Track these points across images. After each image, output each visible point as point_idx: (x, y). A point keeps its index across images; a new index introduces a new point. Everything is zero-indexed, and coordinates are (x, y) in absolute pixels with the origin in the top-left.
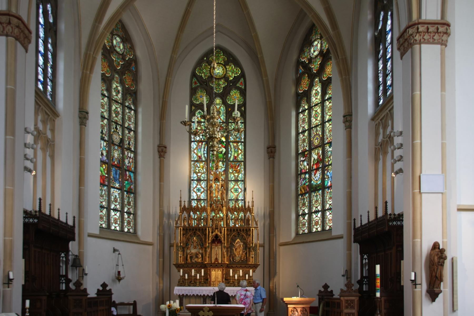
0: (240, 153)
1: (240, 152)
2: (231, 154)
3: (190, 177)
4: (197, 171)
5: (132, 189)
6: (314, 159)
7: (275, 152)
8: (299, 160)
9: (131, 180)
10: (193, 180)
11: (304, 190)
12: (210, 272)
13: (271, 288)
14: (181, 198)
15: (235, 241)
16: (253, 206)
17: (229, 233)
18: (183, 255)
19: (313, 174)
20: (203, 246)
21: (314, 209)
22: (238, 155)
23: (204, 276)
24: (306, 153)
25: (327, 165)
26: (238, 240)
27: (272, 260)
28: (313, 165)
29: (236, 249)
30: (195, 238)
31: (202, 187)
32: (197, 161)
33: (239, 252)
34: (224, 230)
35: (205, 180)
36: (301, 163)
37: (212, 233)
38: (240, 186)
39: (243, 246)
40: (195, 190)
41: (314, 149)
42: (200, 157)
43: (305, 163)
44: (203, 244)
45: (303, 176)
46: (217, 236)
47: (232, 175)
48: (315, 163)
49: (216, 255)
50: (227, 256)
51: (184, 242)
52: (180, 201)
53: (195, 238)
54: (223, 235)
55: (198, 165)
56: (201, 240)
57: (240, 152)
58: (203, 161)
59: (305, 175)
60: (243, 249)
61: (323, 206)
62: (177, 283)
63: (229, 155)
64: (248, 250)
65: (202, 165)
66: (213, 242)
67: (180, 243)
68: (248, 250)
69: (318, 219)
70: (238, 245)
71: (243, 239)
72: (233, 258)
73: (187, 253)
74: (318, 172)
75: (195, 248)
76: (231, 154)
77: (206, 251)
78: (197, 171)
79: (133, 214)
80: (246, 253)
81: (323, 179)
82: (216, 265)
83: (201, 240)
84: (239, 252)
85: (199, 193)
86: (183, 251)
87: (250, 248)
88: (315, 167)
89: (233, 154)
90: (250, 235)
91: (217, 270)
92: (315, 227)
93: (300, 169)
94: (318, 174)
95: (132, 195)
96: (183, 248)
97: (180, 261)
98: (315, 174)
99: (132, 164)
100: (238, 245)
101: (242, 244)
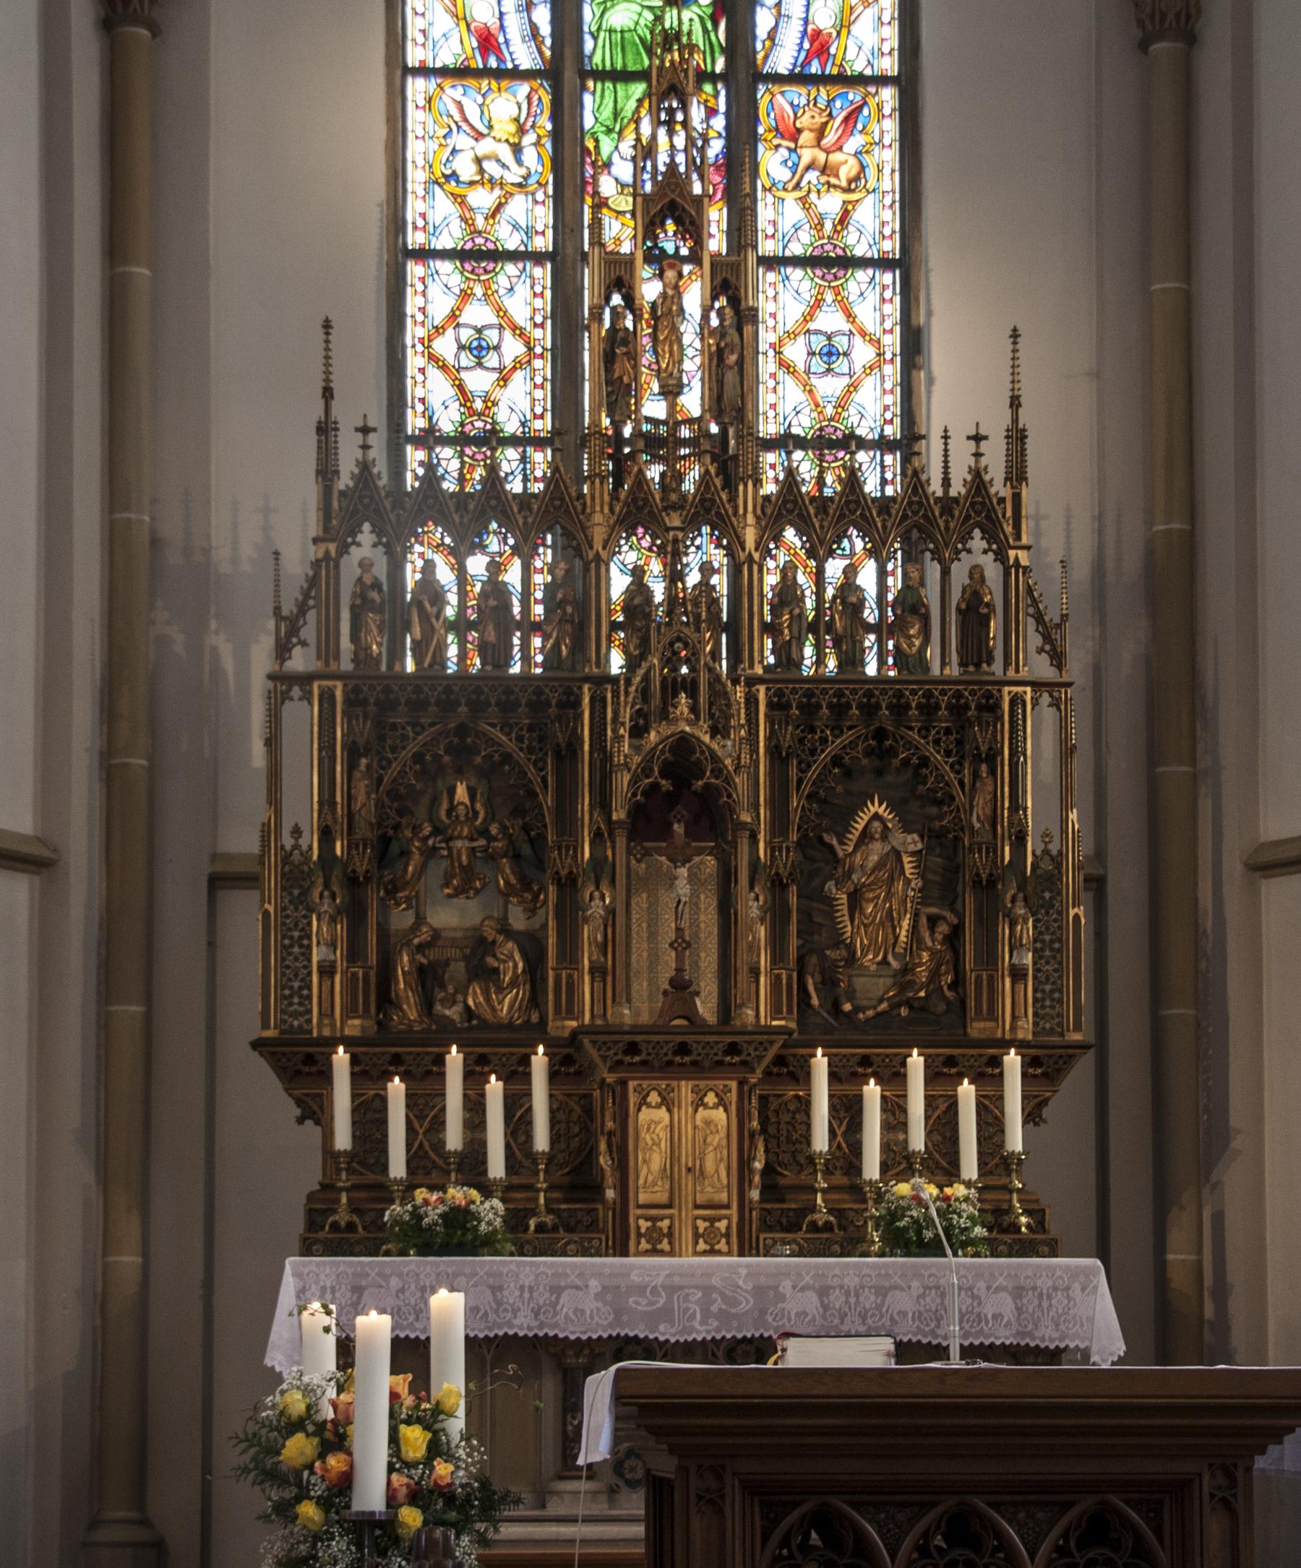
3: (396, 223)
4: (466, 170)
10: (424, 254)
12: (623, 1117)
13: (1179, 1279)
14: (328, 393)
15: (842, 824)
16: (1016, 473)
17: (788, 735)
18: (354, 954)
20: (540, 865)
23: (550, 1158)
26: (877, 808)
27: (1179, 1012)
29: (855, 901)
30: (461, 792)
31: (506, 322)
32: (460, 73)
33: (884, 932)
34: (751, 701)
35: (537, 258)
37: (638, 732)
38: (866, 313)
39: (922, 871)
40: (445, 346)
42: (487, 42)
44: (537, 842)
46: (682, 760)
47: (792, 212)
49: (682, 944)
50: (778, 956)
51: (363, 831)
52: (326, 429)
53: (461, 792)
54: (743, 757)
56: (522, 805)
58: (517, 74)
59: (913, 636)
60: (925, 896)
62: (299, 1225)
64: (969, 903)
66: (648, 822)
67: (326, 835)
68: (969, 903)
70: (876, 851)
71: (926, 806)
72: (828, 982)
73: (383, 932)
77: (569, 915)
78: (466, 170)
80: (957, 931)
82: (679, 1051)
83: (522, 805)
84: (884, 932)
86: (355, 914)
87: (987, 887)
90: (992, 757)
91: (685, 1090)
96: (353, 883)
97: (326, 1013)
100: (876, 851)
101: (913, 842)
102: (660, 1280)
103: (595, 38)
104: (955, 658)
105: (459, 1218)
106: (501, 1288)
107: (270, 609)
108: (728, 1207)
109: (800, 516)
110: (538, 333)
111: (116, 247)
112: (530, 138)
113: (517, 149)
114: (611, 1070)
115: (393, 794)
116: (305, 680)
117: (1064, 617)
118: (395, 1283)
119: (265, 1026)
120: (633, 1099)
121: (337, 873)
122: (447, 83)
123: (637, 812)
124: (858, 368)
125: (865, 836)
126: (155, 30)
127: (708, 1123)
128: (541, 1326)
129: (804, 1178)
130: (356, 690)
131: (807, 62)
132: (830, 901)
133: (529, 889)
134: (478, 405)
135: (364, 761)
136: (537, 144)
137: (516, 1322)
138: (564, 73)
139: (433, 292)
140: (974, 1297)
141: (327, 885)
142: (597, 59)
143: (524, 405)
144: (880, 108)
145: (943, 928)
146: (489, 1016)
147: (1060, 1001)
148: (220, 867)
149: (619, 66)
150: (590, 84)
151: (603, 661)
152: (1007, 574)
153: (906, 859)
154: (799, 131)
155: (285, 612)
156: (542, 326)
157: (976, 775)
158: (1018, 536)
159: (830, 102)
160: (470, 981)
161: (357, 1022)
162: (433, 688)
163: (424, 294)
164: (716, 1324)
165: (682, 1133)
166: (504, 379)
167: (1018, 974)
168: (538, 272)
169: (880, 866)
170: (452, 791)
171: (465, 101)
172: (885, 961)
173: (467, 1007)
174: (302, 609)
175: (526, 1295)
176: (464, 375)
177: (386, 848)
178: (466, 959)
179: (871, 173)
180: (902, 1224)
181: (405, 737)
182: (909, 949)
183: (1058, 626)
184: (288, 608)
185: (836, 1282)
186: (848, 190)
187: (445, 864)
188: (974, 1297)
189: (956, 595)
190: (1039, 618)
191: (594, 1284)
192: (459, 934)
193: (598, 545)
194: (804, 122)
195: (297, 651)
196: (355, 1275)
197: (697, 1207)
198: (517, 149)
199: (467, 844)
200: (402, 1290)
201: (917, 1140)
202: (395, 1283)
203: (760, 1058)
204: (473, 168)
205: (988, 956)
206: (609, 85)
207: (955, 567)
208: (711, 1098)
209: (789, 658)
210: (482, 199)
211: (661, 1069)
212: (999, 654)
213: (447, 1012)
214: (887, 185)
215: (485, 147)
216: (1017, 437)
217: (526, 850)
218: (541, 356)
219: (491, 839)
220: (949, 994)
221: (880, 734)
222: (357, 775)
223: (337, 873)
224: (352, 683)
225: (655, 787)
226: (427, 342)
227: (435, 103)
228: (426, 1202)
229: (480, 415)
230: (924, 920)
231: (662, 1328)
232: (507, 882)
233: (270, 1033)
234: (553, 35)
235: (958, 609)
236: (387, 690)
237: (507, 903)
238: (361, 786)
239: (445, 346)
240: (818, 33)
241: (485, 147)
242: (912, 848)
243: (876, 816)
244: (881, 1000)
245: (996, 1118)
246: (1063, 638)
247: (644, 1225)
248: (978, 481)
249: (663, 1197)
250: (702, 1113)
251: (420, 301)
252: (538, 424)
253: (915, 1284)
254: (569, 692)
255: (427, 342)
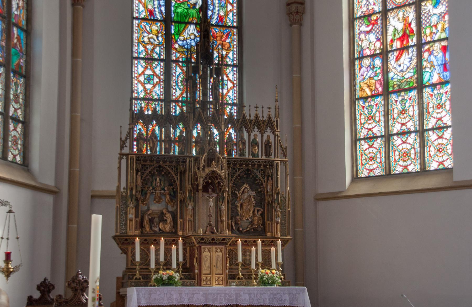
0: (231, 11)
1: (230, 7)
2: (213, 11)
4: (146, 40)
5: (21, 67)
6: (395, 29)
7: (303, 12)
8: (357, 31)
9: (21, 47)
10: (137, 58)
11: (371, 90)
12: (200, 254)
18: (137, 216)
19: (392, 57)
21: (396, 128)
22: (227, 14)
24: (374, 18)
25: (429, 43)
28: (392, 41)
35: (162, 60)
36: (362, 36)
41: (393, 9)
42: (151, 13)
43: (372, 37)
45: (367, 62)
48: (397, 36)
55: (148, 29)
57: (230, 7)
58: (158, 21)
60: (256, 205)
61: (422, 123)
63: (210, 13)
65: (155, 28)
69: (409, 146)
70: (246, 195)
71: (257, 186)
72: (236, 224)
74: (405, 54)
75: (158, 200)
76: (213, 11)
78: (146, 40)
79: (23, 123)
81: (420, 69)
84: (248, 215)
85: (149, 86)
87: (270, 204)
88: (397, 44)
89: (217, 12)
91: (214, 248)
92: (401, 163)
93: (357, 49)
94: (409, 59)
95: (22, 80)
98: (398, 59)
99: (22, 11)
101: (253, 193)
102: (215, 292)
103: (174, 14)
104: (264, 154)
105: (170, 278)
106: (181, 294)
107: (119, 138)
108: (222, 274)
109: (233, 123)
110: (162, 77)
111: (74, 54)
112: (160, 35)
113: (157, 37)
114: (197, 244)
115: (144, 180)
116: (127, 155)
117: (286, 147)
118: (158, 293)
119: (117, 232)
120: (202, 250)
121: (134, 198)
122: (142, 21)
123: (204, 187)
124: (229, 88)
125: (243, 192)
126: (83, 6)
127: (218, 256)
128: (190, 302)
129: (134, 267)
130: (138, 157)
131: (219, 22)
132: (236, 206)
133: (172, 202)
134: (149, 92)
135: (139, 173)
136: (162, 36)
137: (163, 302)
138: (167, 21)
139: (139, 67)
140: (281, 295)
141: (132, 201)
142: (175, 18)
143: (158, 92)
144: (234, 33)
145: (260, 212)
146: (164, 230)
147: (286, 229)
148: (93, 194)
149: (179, 20)
150: (173, 24)
151: (191, 152)
152: (275, 137)
153: (252, 197)
154: (217, 37)
155: (123, 139)
156: (162, 75)
157: (268, 180)
158: (278, 129)
159: (223, 31)
160: (159, 222)
161: (137, 231)
162: (155, 157)
163: (137, 67)
164: (227, 301)
165: (212, 257)
166: (154, 86)
167: (277, 223)
168: (162, 64)
169: (247, 198)
170: (156, 180)
171: (146, 26)
172: (248, 219)
173: (159, 228)
174: (126, 139)
175: (165, 296)
176: (145, 85)
177: (143, 192)
178: (159, 217)
179: (232, 47)
180: (264, 279)
181: (147, 168)
182: (253, 216)
183: (285, 148)
184: (123, 139)
185: (252, 292)
186: (227, 50)
187: (154, 196)
188: (281, 295)
189: (264, 141)
190: (281, 146)
191: (201, 293)
192: (157, 212)
193: (191, 128)
194: (218, 35)
195: (125, 148)
196: (150, 291)
197: (216, 274)
198: (157, 37)
199: (159, 192)
200: (160, 294)
201: (162, 259)
202: (158, 293)
203: (229, 242)
204: (148, 40)
205: (270, 218)
206: (177, 24)
207: (264, 135)
208: (219, 250)
209: (230, 153)
210: (149, 47)
211: (208, 244)
212: (273, 154)
213: (156, 229)
214: (235, 50)
215: (151, 36)
216: (276, 108)
217: (172, 193)
218: (162, 82)
219: (165, 190)
220: (261, 227)
221: (248, 170)
222: (138, 176)
223: (134, 198)
224: (137, 156)
225: (208, 181)
226: (138, 77)
227: (140, 26)
228: (163, 274)
229: (149, 94)
230: (256, 211)
231: (216, 302)
232: (168, 201)
233: (118, 234)
234: (165, 13)
235: (265, 144)
236: (145, 157)
237: (168, 204)
238: (139, 178)
239: (142, 79)
240: (221, 16)
241: (151, 36)
242: (253, 195)
243: (246, 188)
244: (247, 228)
245: (235, 253)
246: (286, 151)
247: (204, 278)
248: (269, 118)
249: (208, 272)
250: (217, 253)
251: (136, 69)
252: (162, 97)
253: (268, 292)
254: (184, 159)
255: (138, 77)
